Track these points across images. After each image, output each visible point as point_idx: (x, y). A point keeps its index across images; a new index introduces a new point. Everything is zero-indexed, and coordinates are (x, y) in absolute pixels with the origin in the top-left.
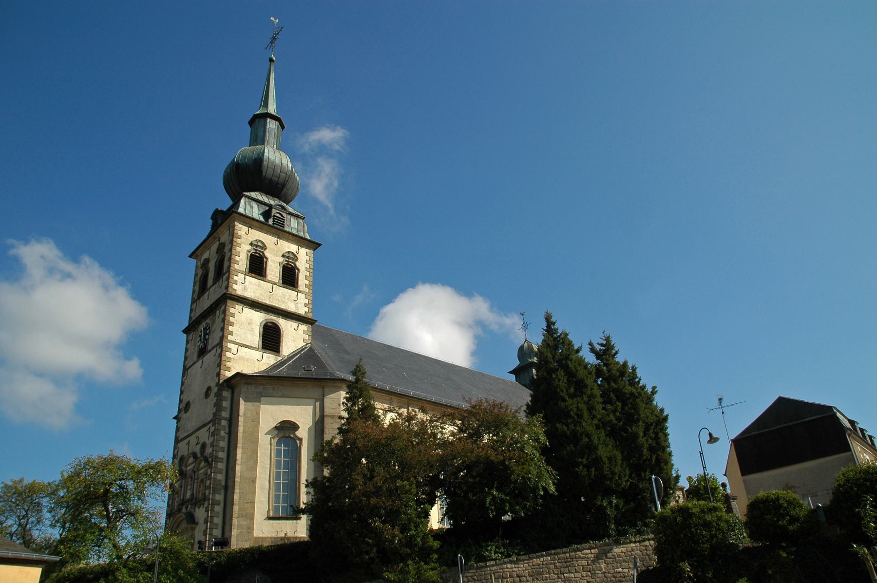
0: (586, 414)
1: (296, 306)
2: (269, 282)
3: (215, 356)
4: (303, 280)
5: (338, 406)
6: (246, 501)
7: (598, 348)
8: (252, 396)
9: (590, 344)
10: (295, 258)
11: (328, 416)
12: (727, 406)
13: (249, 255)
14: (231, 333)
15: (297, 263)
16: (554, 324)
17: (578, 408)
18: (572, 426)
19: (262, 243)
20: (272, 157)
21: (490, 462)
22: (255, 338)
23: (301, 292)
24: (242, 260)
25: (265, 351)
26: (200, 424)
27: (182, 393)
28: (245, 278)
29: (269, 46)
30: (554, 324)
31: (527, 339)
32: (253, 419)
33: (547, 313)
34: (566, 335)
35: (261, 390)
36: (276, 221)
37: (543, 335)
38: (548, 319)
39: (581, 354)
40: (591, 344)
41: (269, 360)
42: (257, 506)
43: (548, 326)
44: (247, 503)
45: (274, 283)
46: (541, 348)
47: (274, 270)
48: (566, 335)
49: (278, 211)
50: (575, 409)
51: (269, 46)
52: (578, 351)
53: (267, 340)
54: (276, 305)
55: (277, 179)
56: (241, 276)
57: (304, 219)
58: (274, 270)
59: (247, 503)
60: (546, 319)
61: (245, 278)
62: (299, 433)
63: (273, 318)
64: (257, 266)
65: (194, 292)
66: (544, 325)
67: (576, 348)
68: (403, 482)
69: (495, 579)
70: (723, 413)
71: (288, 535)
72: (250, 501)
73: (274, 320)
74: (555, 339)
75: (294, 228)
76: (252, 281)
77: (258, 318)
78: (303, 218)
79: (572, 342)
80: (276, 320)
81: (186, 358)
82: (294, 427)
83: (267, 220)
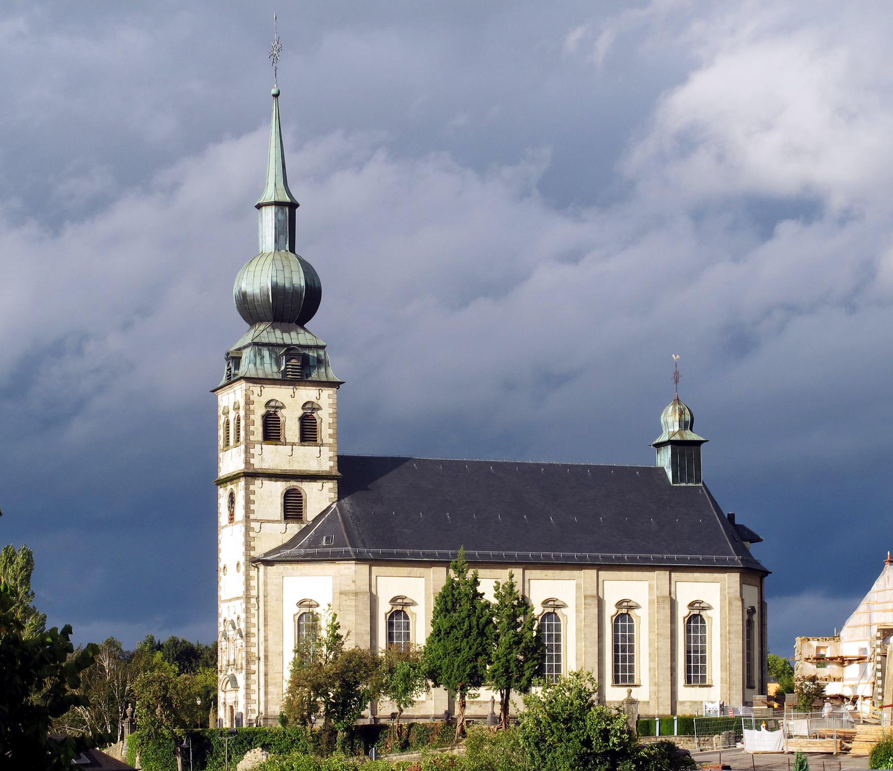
1: (319, 463)
3: (240, 532)
6: (275, 672)
8: (274, 577)
14: (253, 512)
18: (368, 687)
22: (276, 509)
28: (262, 449)
29: (258, 361)
32: (276, 599)
41: (294, 528)
42: (430, 605)
44: (276, 673)
45: (293, 444)
47: (291, 429)
51: (258, 361)
56: (258, 447)
58: (291, 429)
59: (276, 673)
61: (262, 449)
63: (293, 484)
72: (277, 672)
73: (295, 486)
76: (269, 448)
77: (280, 487)
80: (298, 485)
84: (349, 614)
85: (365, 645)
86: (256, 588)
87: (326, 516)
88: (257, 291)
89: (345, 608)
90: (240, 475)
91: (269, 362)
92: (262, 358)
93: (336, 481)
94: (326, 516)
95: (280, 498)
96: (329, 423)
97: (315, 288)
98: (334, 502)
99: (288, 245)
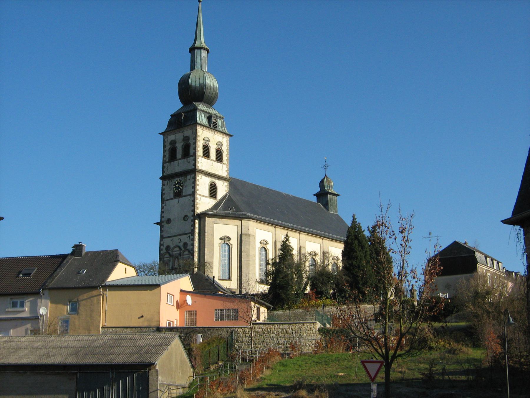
0: (363, 258)
2: (212, 160)
4: (225, 158)
5: (248, 230)
7: (371, 229)
9: (368, 228)
10: (222, 145)
11: (244, 234)
12: (433, 237)
13: (203, 145)
15: (222, 148)
16: (356, 219)
17: (361, 256)
19: (209, 139)
20: (209, 83)
21: (475, 347)
22: (207, 192)
23: (224, 164)
24: (200, 149)
25: (212, 198)
26: (181, 233)
27: (162, 212)
30: (356, 219)
31: (327, 175)
33: (354, 214)
34: (360, 224)
35: (214, 220)
36: (214, 124)
37: (351, 223)
38: (353, 217)
39: (364, 233)
40: (368, 227)
43: (353, 220)
45: (213, 161)
46: (350, 230)
48: (360, 224)
49: (215, 119)
50: (360, 256)
52: (363, 231)
53: (211, 192)
54: (215, 173)
55: (211, 95)
56: (200, 158)
57: (223, 119)
60: (353, 217)
62: (231, 242)
64: (206, 153)
65: (164, 156)
66: (352, 219)
67: (362, 230)
68: (345, 284)
69: (290, 321)
70: (430, 240)
71: (228, 287)
73: (213, 181)
74: (355, 225)
75: (220, 126)
76: (205, 160)
78: (223, 118)
79: (361, 227)
81: (163, 194)
82: (229, 238)
83: (210, 125)
84: (247, 245)
85: (166, 326)
86: (179, 237)
87: (226, 198)
88: (198, 85)
89: (245, 242)
90: (222, 178)
91: (204, 119)
92: (202, 116)
93: (228, 182)
94: (226, 198)
95: (208, 186)
96: (226, 154)
97: (460, 359)
98: (227, 192)
99: (206, 69)
